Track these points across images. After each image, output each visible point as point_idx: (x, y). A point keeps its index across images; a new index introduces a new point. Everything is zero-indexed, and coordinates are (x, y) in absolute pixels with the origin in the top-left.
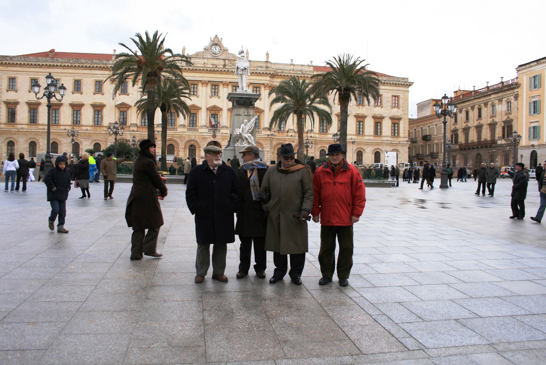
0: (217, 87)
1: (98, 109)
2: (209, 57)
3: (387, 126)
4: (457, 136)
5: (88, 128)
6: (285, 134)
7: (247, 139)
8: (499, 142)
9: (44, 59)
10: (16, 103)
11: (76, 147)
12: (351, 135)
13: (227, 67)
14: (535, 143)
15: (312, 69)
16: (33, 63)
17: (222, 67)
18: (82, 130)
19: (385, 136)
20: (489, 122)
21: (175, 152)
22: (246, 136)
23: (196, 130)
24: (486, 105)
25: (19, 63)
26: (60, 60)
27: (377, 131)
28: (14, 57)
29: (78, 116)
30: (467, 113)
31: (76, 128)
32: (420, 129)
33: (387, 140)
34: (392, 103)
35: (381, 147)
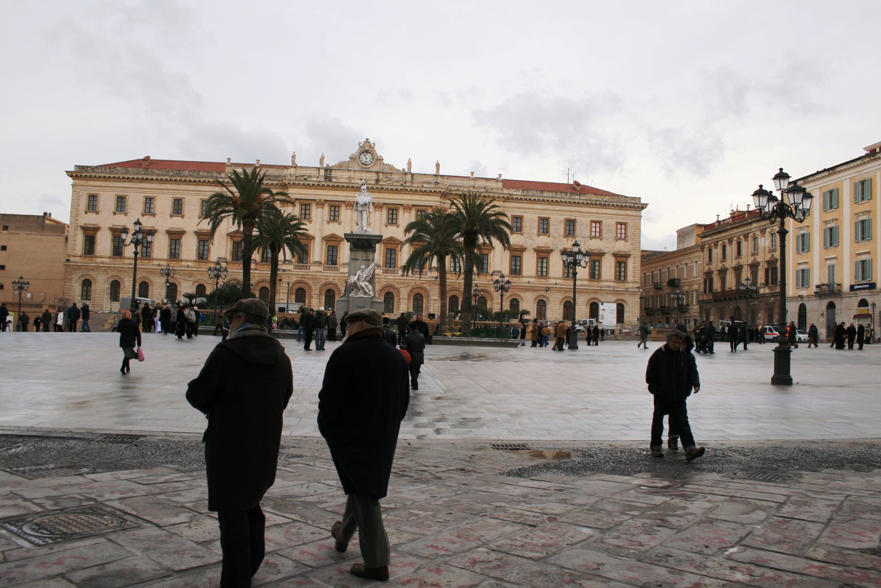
0: (395, 212)
1: (175, 237)
2: (356, 169)
3: (608, 267)
4: (711, 280)
5: (190, 264)
6: (489, 278)
7: (363, 288)
8: (762, 291)
9: (135, 170)
10: (97, 229)
11: (172, 290)
12: (581, 280)
13: (381, 183)
14: (804, 292)
15: (500, 185)
16: (121, 176)
17: (374, 182)
18: (181, 266)
19: (606, 281)
20: (750, 262)
21: (307, 300)
22: (363, 284)
23: (337, 269)
24: (746, 237)
25: (102, 175)
26: (156, 171)
27: (543, 272)
28: (97, 167)
29: (177, 247)
30: (724, 247)
31: (174, 265)
32: (666, 270)
33: (609, 287)
34: (617, 233)
35: (599, 296)
